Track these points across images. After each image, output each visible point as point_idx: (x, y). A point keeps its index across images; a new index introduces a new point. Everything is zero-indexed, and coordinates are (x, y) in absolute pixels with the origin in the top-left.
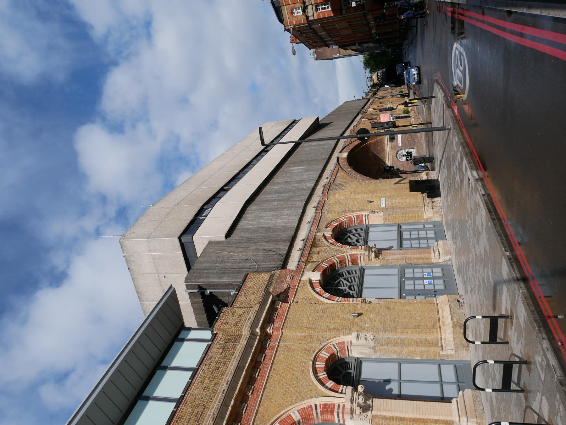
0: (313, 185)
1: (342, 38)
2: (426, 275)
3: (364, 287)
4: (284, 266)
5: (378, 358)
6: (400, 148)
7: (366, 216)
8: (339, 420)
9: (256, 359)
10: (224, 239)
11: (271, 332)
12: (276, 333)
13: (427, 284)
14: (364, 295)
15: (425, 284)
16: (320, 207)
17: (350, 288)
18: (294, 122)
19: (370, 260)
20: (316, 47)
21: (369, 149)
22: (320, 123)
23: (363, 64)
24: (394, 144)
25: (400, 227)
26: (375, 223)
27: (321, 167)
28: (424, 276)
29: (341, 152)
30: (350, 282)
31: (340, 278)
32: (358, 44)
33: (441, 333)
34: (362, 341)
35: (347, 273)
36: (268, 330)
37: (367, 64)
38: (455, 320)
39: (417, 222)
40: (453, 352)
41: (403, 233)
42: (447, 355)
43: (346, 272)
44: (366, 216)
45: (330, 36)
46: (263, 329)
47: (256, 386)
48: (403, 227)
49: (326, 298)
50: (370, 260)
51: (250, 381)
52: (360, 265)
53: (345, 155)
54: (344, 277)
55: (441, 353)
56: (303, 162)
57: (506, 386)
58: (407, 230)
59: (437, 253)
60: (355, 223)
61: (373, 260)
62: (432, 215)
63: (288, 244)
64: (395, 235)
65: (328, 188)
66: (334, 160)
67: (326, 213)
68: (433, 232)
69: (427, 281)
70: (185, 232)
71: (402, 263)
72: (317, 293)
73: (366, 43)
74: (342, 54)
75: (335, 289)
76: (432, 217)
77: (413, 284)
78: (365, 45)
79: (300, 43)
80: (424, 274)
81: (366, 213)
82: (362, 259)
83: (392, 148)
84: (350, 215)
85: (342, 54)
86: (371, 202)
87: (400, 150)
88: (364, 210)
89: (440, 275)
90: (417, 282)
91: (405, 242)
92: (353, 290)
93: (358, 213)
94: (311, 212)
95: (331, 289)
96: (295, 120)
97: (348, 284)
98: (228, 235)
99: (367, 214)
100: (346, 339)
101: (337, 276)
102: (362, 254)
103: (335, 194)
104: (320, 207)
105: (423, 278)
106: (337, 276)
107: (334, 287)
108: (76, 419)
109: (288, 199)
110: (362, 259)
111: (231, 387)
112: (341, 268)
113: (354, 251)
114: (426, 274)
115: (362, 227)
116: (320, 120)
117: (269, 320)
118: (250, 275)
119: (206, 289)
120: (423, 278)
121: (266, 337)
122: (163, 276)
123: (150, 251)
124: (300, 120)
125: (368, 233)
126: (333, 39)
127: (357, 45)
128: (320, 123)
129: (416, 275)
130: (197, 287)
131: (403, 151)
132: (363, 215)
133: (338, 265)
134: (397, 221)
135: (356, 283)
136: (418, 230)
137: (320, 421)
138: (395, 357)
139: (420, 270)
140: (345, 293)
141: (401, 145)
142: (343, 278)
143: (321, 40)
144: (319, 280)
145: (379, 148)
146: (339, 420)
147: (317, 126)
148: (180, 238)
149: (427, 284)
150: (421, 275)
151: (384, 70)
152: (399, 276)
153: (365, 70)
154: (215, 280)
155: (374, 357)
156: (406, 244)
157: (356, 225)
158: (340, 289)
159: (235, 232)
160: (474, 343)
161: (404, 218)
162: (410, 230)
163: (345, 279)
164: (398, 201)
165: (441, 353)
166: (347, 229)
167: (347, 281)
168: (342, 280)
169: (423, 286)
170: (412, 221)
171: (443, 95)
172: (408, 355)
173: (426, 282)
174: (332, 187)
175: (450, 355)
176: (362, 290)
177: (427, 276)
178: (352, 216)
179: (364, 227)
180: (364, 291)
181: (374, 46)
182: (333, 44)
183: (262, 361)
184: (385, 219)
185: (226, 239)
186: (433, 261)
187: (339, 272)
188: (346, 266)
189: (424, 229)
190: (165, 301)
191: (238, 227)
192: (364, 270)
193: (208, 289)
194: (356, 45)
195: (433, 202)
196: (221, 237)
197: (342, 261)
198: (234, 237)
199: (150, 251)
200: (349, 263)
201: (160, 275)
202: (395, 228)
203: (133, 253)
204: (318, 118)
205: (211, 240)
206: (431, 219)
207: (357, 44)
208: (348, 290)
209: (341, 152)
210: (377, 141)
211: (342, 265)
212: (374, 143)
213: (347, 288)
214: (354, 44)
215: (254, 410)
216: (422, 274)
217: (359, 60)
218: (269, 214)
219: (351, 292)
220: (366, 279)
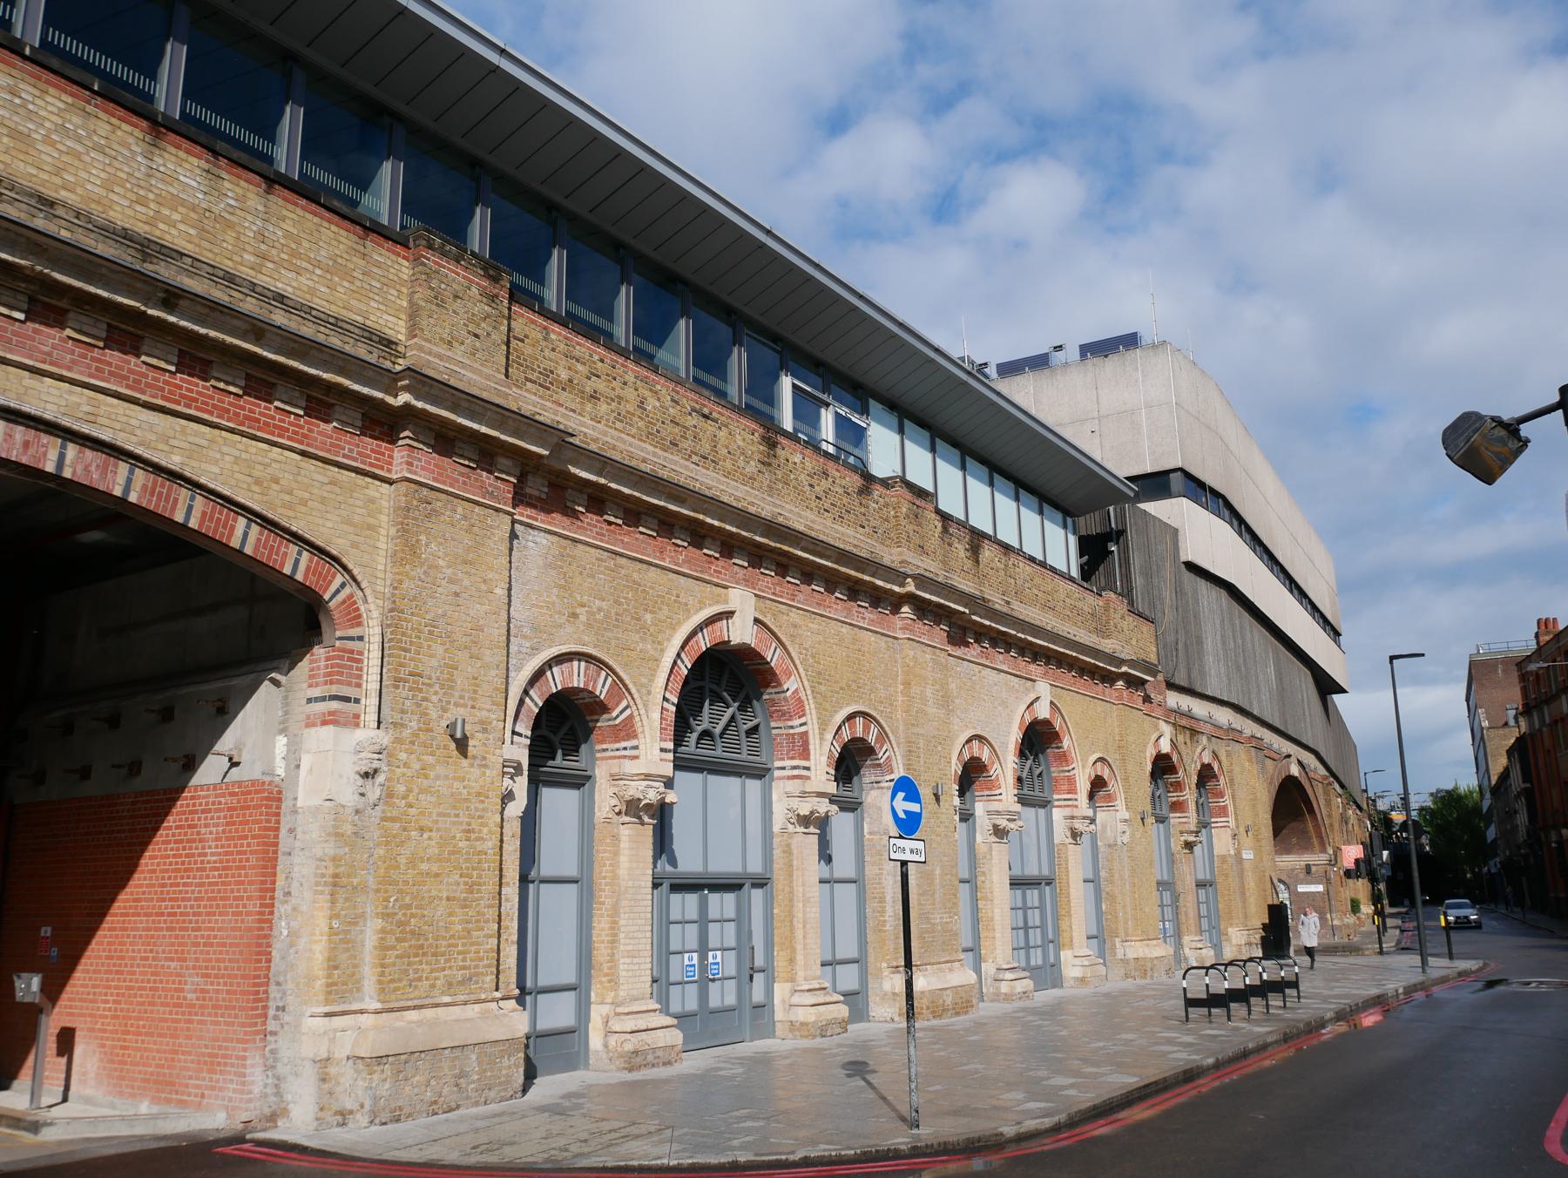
0: (1255, 713)
1: (1549, 751)
2: (715, 957)
3: (709, 776)
4: (1171, 686)
5: (1097, 849)
6: (1292, 887)
7: (1075, 803)
8: (1058, 800)
9: (768, 558)
10: (1183, 558)
11: (903, 615)
12: (899, 624)
13: (686, 962)
14: (683, 778)
15: (686, 955)
16: (1233, 735)
17: (706, 734)
18: (1335, 633)
19: (1181, 833)
20: (1524, 681)
21: (1294, 820)
22: (1328, 697)
23: (1449, 786)
24: (1302, 876)
25: (761, 883)
26: (1215, 840)
27: (1277, 724)
28: (710, 954)
29: (1300, 762)
30: (722, 735)
31: (736, 704)
32: (1525, 789)
33: (328, 1015)
34: (1121, 827)
35: (750, 724)
36: (1121, 683)
37: (1449, 800)
38: (1155, 962)
39: (1219, 917)
40: (1120, 955)
41: (1036, 891)
42: (1113, 947)
43: (756, 721)
44: (805, 773)
45: (1556, 722)
46: (910, 599)
47: (719, 563)
48: (757, 895)
49: (675, 663)
50: (1181, 833)
51: (667, 525)
52: (1171, 815)
53: (1295, 770)
54: (739, 717)
55: (1117, 940)
56: (1281, 679)
57: (1191, 1003)
58: (1042, 898)
59: (1199, 946)
60: (778, 728)
61: (1182, 839)
62: (1234, 942)
63: (1183, 683)
64: (725, 864)
65: (1258, 745)
66: (1289, 747)
67: (1230, 748)
68: (1040, 962)
69: (695, 961)
70: (1188, 476)
71: (1180, 889)
72: (693, 634)
73: (1528, 810)
74: (1488, 736)
75: (701, 688)
76: (1231, 942)
77: (687, 918)
78: (1521, 807)
79: (1538, 643)
80: (719, 953)
81: (1232, 824)
82: (1184, 820)
83: (1293, 870)
84: (1228, 793)
85: (1488, 736)
86: (1142, 819)
87: (1288, 888)
88: (1236, 820)
89: (714, 1002)
90: (692, 930)
91: (692, 899)
92: (698, 743)
93: (1231, 809)
94: (1224, 716)
95: (703, 679)
96: (1339, 635)
97: (718, 730)
98: (1192, 567)
99: (1230, 824)
100: (1120, 803)
101: (742, 696)
102: (1075, 803)
103: (1250, 760)
104: (1233, 735)
105: (703, 950)
106: (742, 696)
107: (708, 685)
108: (536, 81)
109: (1238, 668)
110: (1184, 820)
111: (750, 519)
112: (1166, 784)
113: (1192, 806)
114: (719, 959)
115: (764, 753)
116: (1335, 697)
117: (924, 610)
118: (1146, 628)
119: (1117, 543)
120: (703, 950)
121: (1108, 678)
122: (1096, 428)
123: (1149, 406)
124: (1339, 647)
125: (739, 775)
126: (1545, 729)
127: (1523, 786)
128: (1328, 697)
129: (713, 929)
130: (1120, 527)
131: (1287, 895)
132: (1076, 793)
133: (1172, 778)
134: (1220, 879)
135: (719, 752)
136: (1043, 926)
137: (1054, 775)
138: (1103, 874)
139: (731, 941)
140: (691, 719)
141: (1299, 890)
142: (737, 713)
143: (1544, 698)
144: (729, 641)
145: (1294, 840)
146: (1058, 800)
147: (1326, 686)
148: (1181, 469)
149: (686, 962)
150: (713, 941)
151: (1427, 848)
152: (700, 874)
153: (1432, 794)
154: (1136, 561)
155: (1099, 843)
156: (1202, 892)
157: (774, 732)
158: (702, 707)
159: (1192, 576)
160: (1184, 978)
161: (1227, 892)
162: (1042, 908)
163: (733, 718)
164: (1251, 883)
165: (1117, 940)
166: (759, 698)
167: (728, 725)
168: (730, 711)
169: (679, 948)
170: (1220, 906)
171: (1473, 969)
172: (1107, 893)
173: (691, 959)
174: (1261, 754)
175: (1115, 953)
176: (700, 770)
177: (711, 960)
178: (1226, 797)
179: (1045, 795)
180: (696, 778)
181: (1515, 828)
182: (1530, 724)
183: (762, 570)
184: (1223, 858)
185: (1184, 563)
186: (1186, 939)
187: (755, 702)
188: (1169, 792)
189: (1046, 942)
190: (422, 8)
191: (1198, 579)
192: (760, 777)
193: (1119, 547)
194: (1524, 782)
195: (1257, 944)
196: (1189, 553)
197: (1178, 786)
198: (1188, 576)
199: (1149, 406)
200: (1173, 797)
201: (1097, 422)
202: (755, 867)
203: (1142, 371)
204: (1344, 691)
205: (1181, 533)
206: (1227, 940)
207: (1528, 785)
208: (700, 729)
209: (1300, 762)
210: (1310, 838)
211: (1172, 785)
212: (1305, 832)
213: (705, 725)
214: (1526, 777)
215: (602, 541)
216: (719, 946)
217: (1467, 780)
218: (1219, 637)
219: (694, 736)
220: (733, 783)
